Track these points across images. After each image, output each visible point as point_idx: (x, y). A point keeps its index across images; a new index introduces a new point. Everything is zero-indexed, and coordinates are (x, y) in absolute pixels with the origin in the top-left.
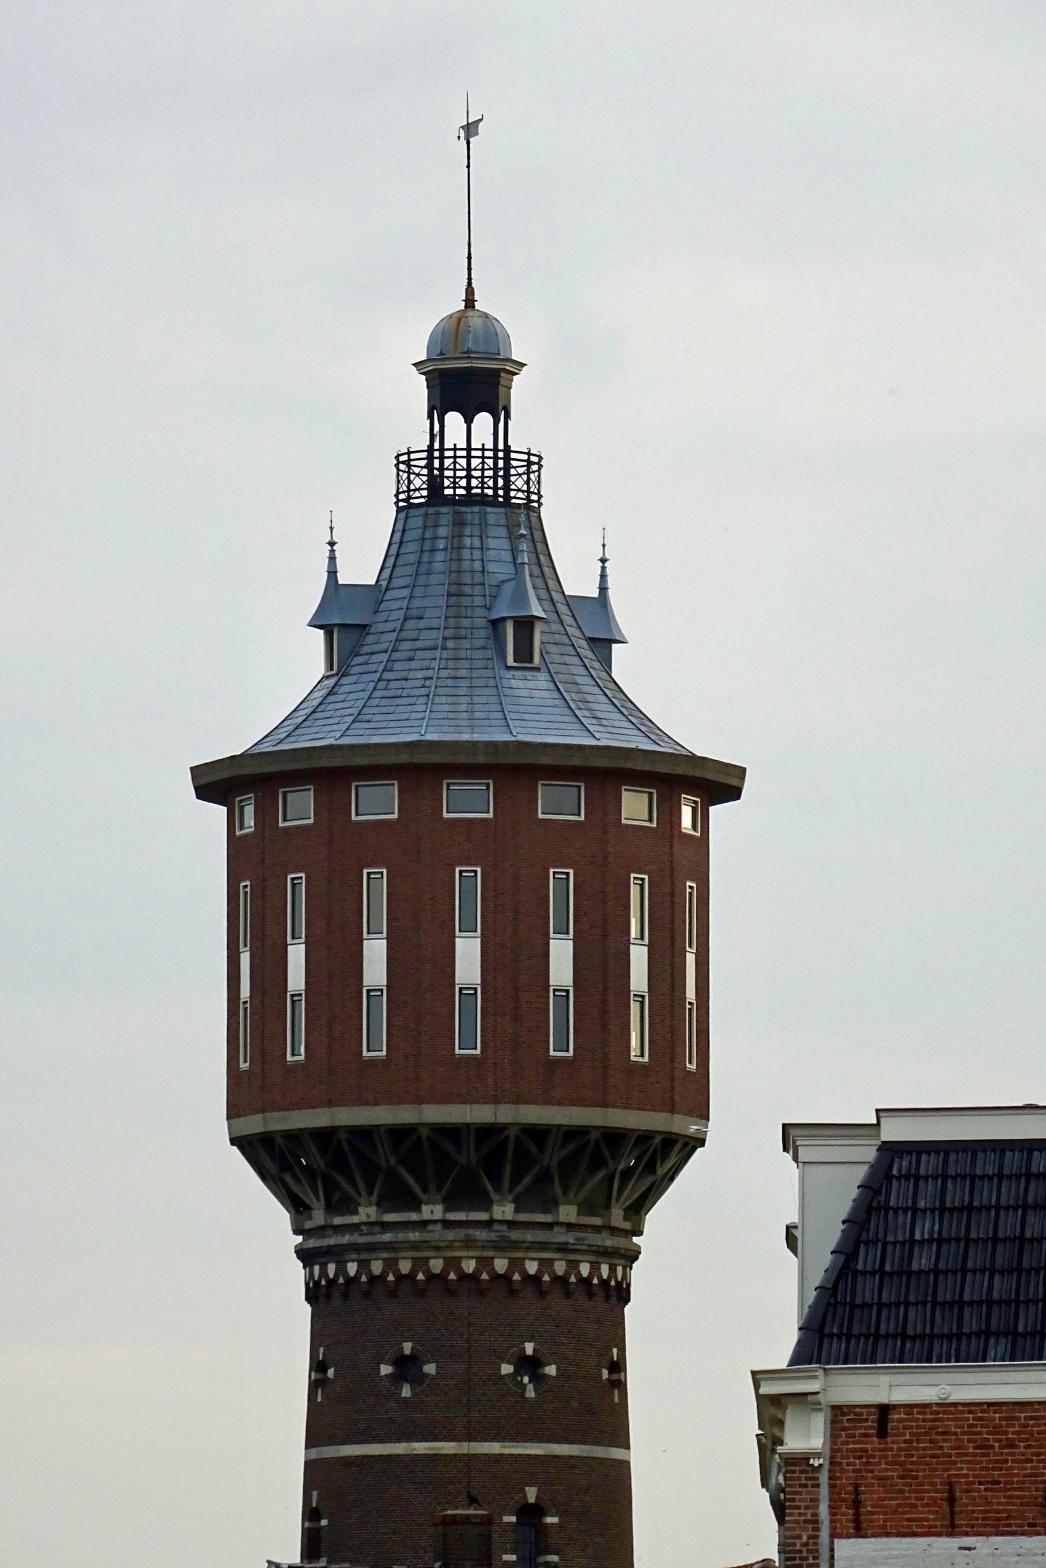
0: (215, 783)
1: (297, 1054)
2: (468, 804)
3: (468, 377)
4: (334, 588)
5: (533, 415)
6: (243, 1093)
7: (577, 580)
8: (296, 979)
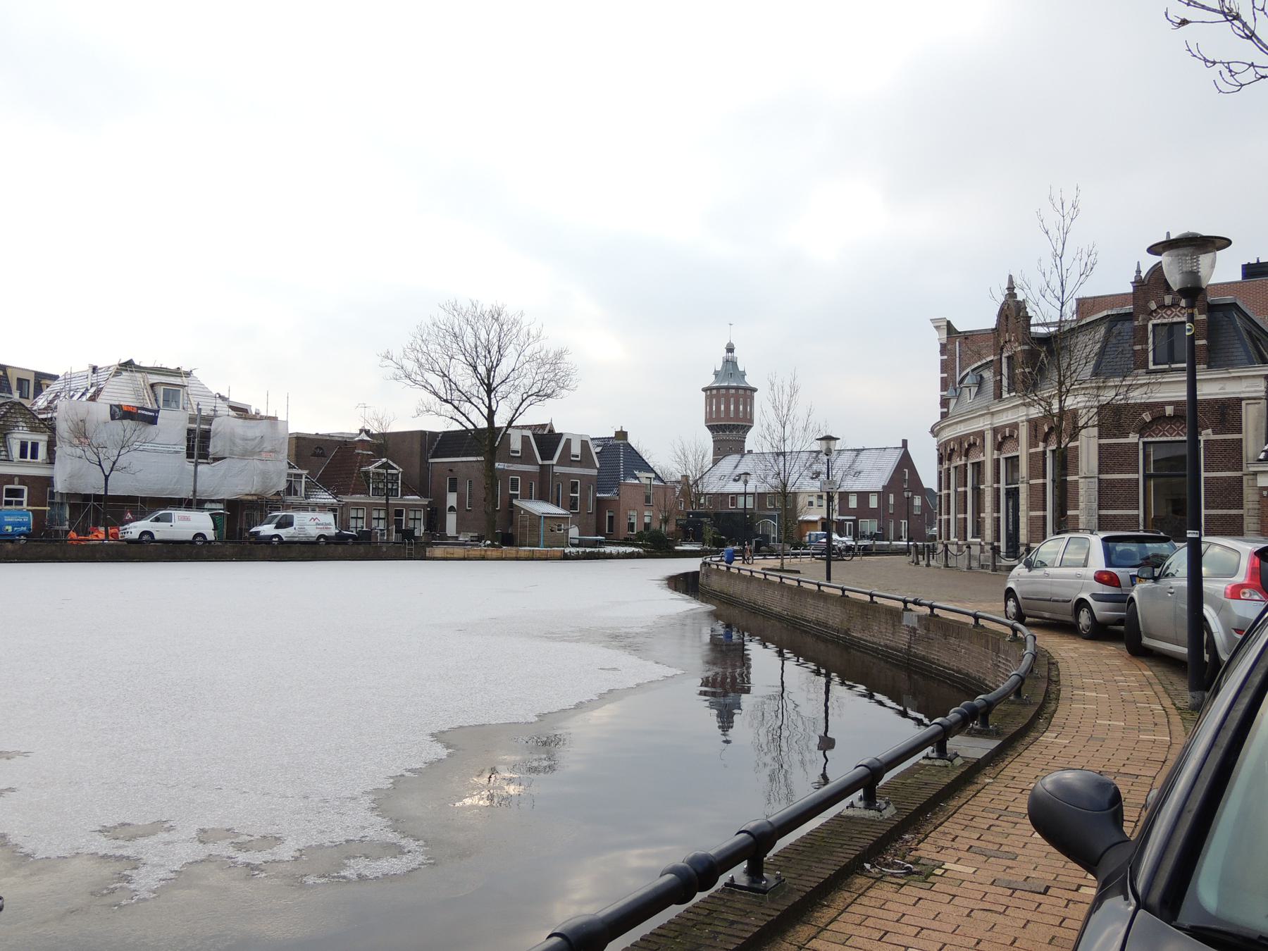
0: (705, 390)
2: (741, 392)
3: (730, 349)
5: (736, 353)
7: (741, 369)
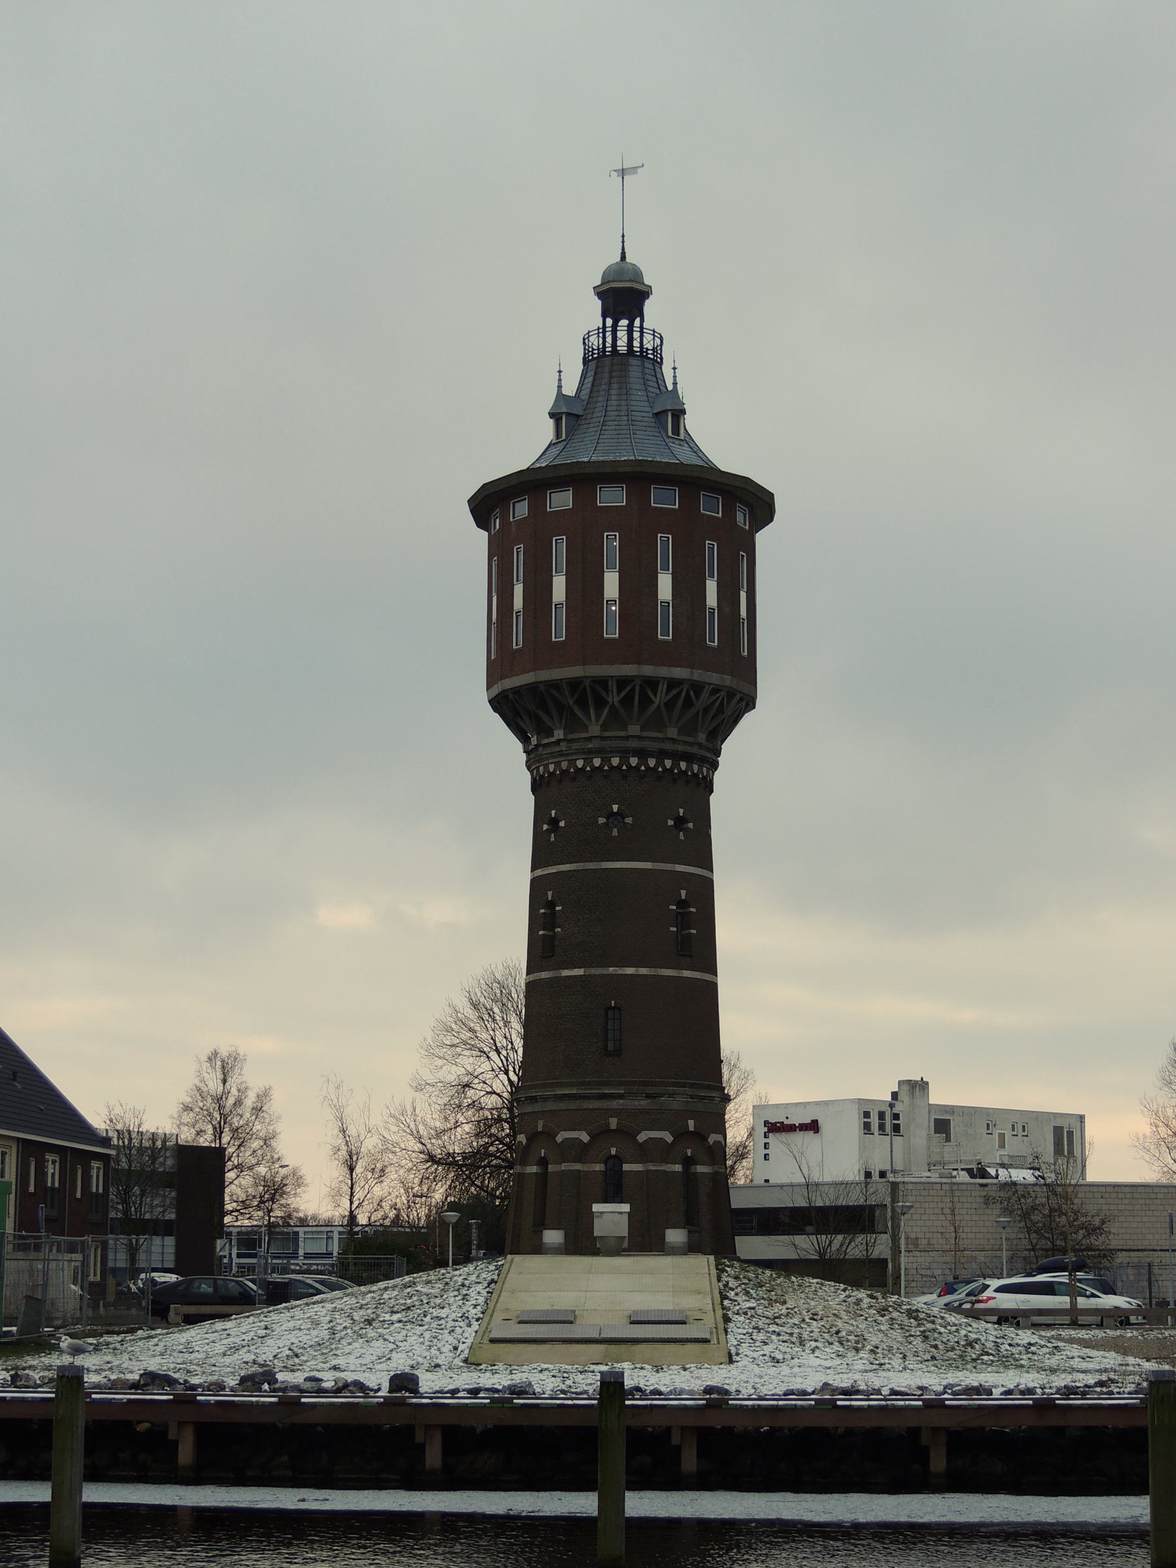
1: (32, 1189)
3: (623, 297)
4: (560, 397)
6: (495, 672)
8: (518, 602)
